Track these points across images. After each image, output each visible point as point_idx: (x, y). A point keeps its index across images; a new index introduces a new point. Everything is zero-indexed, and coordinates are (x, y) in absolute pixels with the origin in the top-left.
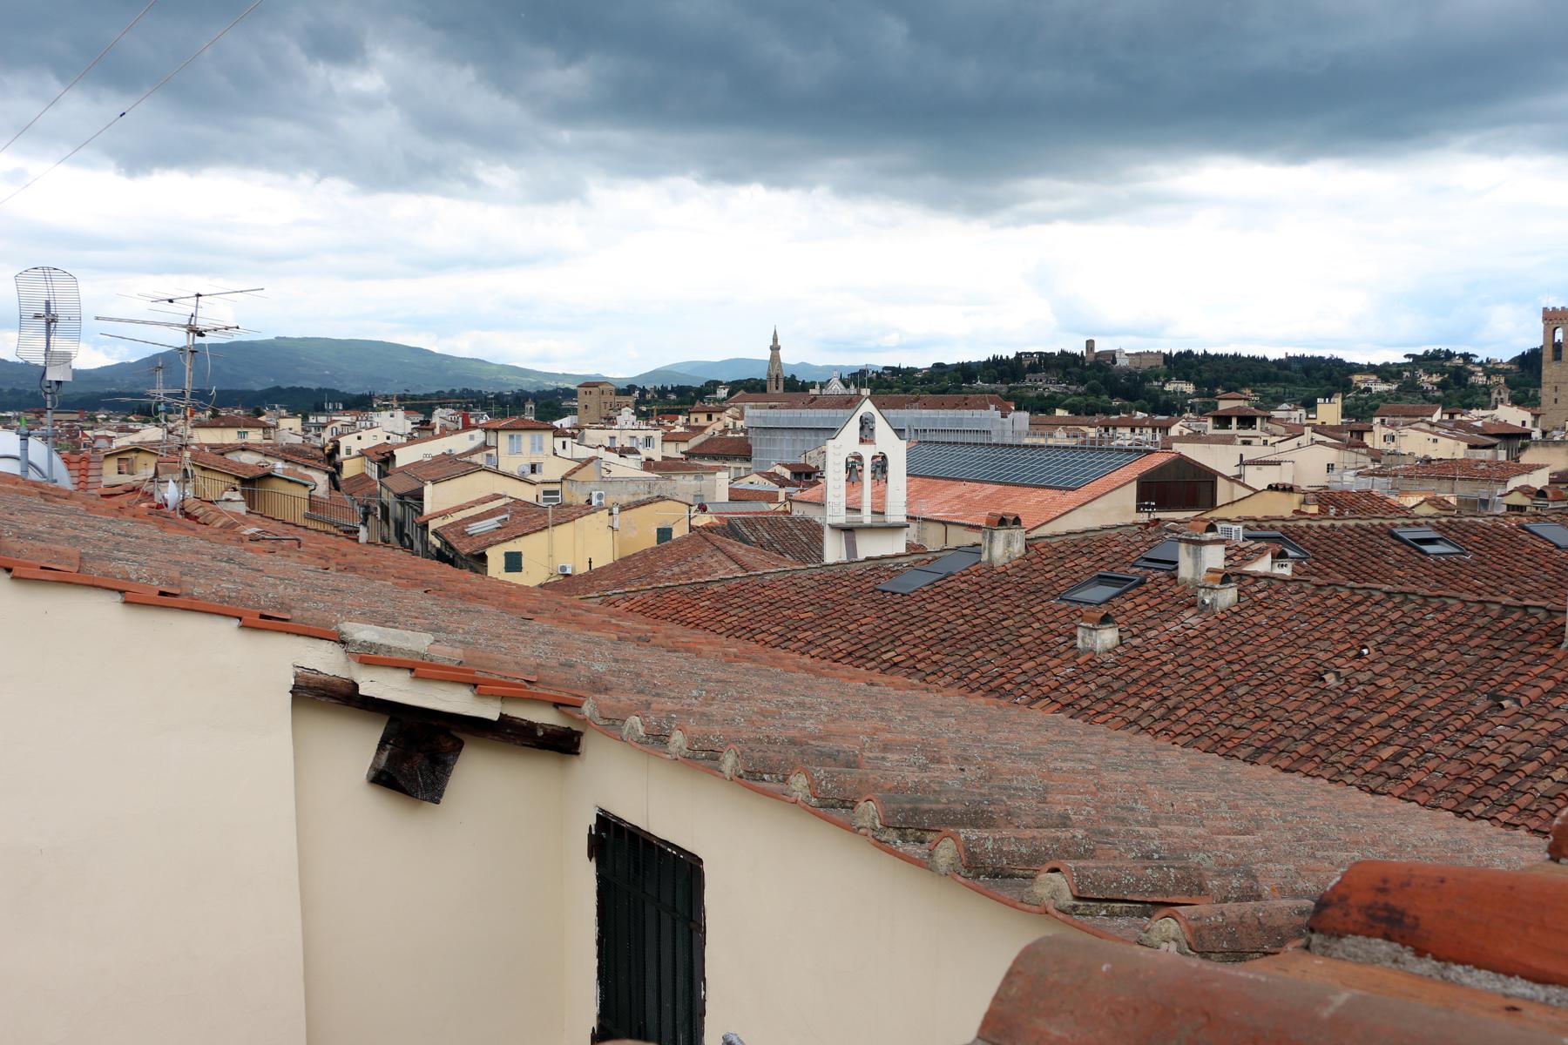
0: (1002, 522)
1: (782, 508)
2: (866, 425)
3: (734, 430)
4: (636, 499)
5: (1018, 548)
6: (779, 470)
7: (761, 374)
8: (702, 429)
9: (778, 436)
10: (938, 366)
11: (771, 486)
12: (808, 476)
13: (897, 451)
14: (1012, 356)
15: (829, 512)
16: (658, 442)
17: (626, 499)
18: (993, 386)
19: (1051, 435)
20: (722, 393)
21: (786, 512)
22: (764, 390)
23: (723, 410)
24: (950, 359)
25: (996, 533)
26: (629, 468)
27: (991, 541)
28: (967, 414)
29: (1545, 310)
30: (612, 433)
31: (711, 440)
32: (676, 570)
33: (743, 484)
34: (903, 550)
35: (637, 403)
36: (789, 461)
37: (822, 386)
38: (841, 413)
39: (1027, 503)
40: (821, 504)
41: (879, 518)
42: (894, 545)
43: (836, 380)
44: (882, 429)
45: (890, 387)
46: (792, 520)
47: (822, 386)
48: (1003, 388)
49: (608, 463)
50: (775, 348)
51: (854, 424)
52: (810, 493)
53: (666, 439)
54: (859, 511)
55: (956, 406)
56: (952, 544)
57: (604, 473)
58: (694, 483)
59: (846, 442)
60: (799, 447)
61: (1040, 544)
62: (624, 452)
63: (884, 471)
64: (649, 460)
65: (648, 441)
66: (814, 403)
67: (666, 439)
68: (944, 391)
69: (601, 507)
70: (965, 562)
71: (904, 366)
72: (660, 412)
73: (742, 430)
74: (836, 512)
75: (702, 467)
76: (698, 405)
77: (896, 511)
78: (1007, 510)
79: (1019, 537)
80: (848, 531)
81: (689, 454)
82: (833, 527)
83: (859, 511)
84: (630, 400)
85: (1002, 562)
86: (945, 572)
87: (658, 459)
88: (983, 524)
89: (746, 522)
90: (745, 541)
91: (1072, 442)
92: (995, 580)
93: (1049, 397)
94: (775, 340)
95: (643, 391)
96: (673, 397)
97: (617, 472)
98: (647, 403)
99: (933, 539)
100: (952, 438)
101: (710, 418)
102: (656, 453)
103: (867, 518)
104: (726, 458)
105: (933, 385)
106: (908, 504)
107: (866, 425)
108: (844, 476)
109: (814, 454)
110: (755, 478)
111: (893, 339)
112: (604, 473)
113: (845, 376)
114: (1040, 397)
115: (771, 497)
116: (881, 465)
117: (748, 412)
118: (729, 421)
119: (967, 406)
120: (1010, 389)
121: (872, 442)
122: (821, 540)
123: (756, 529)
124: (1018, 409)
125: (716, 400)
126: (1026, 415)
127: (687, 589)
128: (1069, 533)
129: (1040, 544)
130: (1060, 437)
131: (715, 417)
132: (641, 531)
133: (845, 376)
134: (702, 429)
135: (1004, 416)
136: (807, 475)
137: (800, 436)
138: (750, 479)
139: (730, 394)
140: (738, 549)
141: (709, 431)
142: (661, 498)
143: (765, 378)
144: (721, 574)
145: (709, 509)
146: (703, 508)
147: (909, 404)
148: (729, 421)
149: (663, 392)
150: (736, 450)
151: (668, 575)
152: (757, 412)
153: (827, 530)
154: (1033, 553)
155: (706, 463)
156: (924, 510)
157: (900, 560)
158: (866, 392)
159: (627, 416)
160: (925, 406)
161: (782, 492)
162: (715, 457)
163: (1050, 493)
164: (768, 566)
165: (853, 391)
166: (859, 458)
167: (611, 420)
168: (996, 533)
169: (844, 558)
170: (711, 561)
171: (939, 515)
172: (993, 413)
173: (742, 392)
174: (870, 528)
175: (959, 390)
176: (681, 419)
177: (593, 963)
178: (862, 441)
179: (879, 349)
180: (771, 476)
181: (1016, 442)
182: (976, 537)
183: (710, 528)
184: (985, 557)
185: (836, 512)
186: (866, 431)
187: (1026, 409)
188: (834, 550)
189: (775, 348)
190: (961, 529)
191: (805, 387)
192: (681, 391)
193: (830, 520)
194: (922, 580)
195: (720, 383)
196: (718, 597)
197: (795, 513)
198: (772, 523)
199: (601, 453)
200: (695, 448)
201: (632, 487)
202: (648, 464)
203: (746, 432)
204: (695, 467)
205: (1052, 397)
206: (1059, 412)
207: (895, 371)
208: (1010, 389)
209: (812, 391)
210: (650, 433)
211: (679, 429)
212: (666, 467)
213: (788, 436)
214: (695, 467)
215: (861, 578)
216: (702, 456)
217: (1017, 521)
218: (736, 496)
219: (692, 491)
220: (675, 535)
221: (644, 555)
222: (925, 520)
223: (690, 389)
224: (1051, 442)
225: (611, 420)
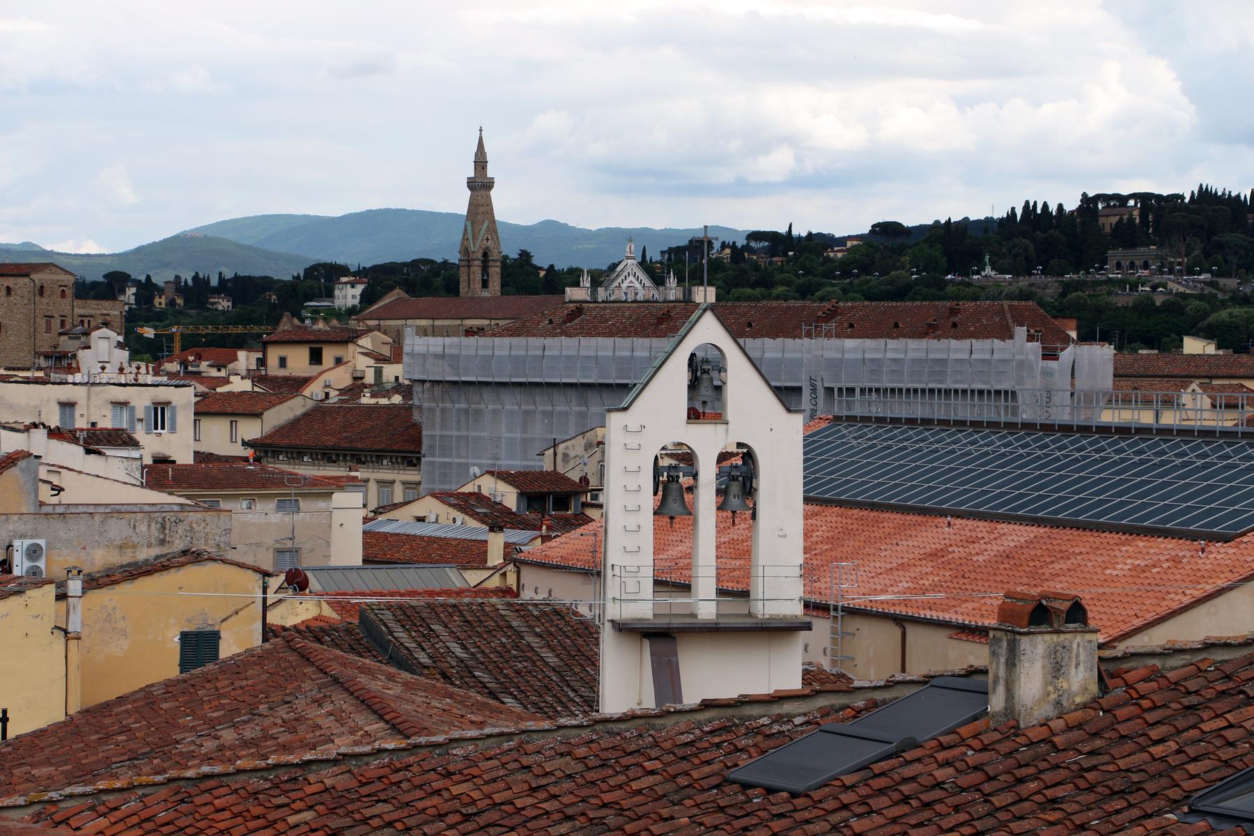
0: (1040, 615)
1: (495, 582)
2: (705, 383)
3: (379, 388)
4: (126, 559)
5: (1080, 680)
6: (488, 486)
7: (445, 249)
8: (297, 384)
9: (488, 403)
10: (887, 231)
11: (469, 527)
12: (562, 501)
13: (779, 441)
14: (1072, 205)
15: (612, 589)
16: (185, 418)
17: (100, 558)
18: (1024, 282)
19: (1168, 403)
20: (348, 295)
21: (505, 592)
22: (452, 288)
23: (350, 338)
24: (916, 212)
25: (1025, 643)
26: (109, 480)
27: (1012, 663)
28: (955, 349)
29: (1084, 195)
30: (65, 393)
31: (319, 413)
32: (228, 736)
33: (401, 522)
34: (794, 683)
35: (132, 320)
36: (515, 464)
37: (598, 279)
38: (642, 346)
39: (1112, 573)
40: (593, 572)
41: (734, 607)
42: (777, 672)
43: (631, 265)
44: (743, 386)
45: (766, 282)
46: (521, 610)
47: (598, 279)
48: (1048, 285)
49: (57, 469)
50: (480, 185)
51: (675, 375)
52: (566, 545)
53: (205, 409)
54: (686, 588)
55: (929, 331)
56: (916, 671)
57: (45, 493)
58: (276, 518)
59: (656, 417)
60: (538, 430)
61: (1136, 671)
62: (96, 441)
63: (749, 490)
64: (161, 461)
65: (160, 415)
66: (577, 321)
67: (205, 409)
68: (901, 293)
69: (36, 580)
70: (946, 714)
71: (800, 231)
72: (190, 343)
73: (398, 388)
74: (630, 594)
75: (295, 479)
76: (287, 324)
77: (780, 590)
78: (1058, 586)
79: (1081, 650)
80: (662, 638)
81: (264, 448)
82: (623, 628)
83: (686, 588)
84: (115, 310)
85: (1047, 710)
86: (897, 739)
87: (184, 457)
88: (991, 622)
89: (407, 616)
90: (402, 661)
91: (1228, 421)
92: (1024, 760)
93: (1167, 306)
94: (481, 162)
95: (147, 289)
96: (224, 304)
97: (77, 491)
98: (156, 318)
99: (872, 658)
100: (919, 409)
101: (316, 358)
102: (180, 445)
103: (706, 606)
104: (358, 457)
105: (874, 279)
106: (809, 572)
107: (705, 383)
108: (648, 501)
109: (576, 447)
110: (429, 507)
111: (779, 162)
112: (45, 493)
113: (654, 255)
114: (1144, 308)
115: (473, 555)
116: (740, 474)
117: (414, 343)
118: (364, 365)
119: (957, 330)
120: (1068, 288)
121: (718, 417)
122: (593, 661)
123: (431, 635)
124: (1086, 337)
125: (332, 313)
126: (1105, 352)
127: (256, 783)
128: (1209, 646)
129: (1136, 671)
130: (1195, 408)
131: (329, 354)
132: (140, 641)
133: (654, 255)
134: (297, 384)
135: (1050, 355)
136: (560, 501)
137: (541, 404)
138: (418, 509)
139: (368, 298)
140: (384, 683)
141: (315, 390)
142: (193, 557)
143: (454, 258)
144: (343, 745)
145: (314, 584)
146: (297, 581)
147: (813, 326)
148: (364, 365)
149: (197, 292)
150: (379, 438)
151: (207, 749)
152: (435, 344)
153: (608, 637)
154: (1119, 693)
155: (307, 470)
156: (849, 587)
157: (787, 708)
158: (705, 294)
159: (105, 349)
160: (852, 330)
161: (496, 544)
162: (328, 455)
163: (1168, 546)
164: (460, 725)
165: (673, 290)
166: (687, 458)
167: (61, 363)
168: (1025, 643)
169: (650, 703)
170: (317, 714)
171: (885, 599)
172: (1021, 346)
173: (397, 293)
174: (713, 631)
175: (936, 290)
176: (245, 359)
177: (409, 207)
178: (694, 415)
179: (743, 189)
180: (469, 503)
181: (1081, 419)
182: (975, 654)
183: (315, 631)
184: (997, 702)
185: (630, 594)
186: (705, 392)
187: (1105, 338)
188: (623, 684)
189: (480, 185)
190: (940, 636)
191: (556, 281)
192: (246, 290)
193: (614, 611)
194: (837, 759)
195: (342, 270)
196: (334, 801)
197: (527, 595)
198: (472, 617)
199: (38, 442)
200: (281, 431)
201: (117, 530)
202: (159, 472)
203: (407, 391)
204: (278, 480)
205: (1176, 306)
206: (1193, 346)
207: (779, 242)
208: (1068, 288)
209: (572, 293)
210: (164, 394)
211: (240, 385)
212: (207, 478)
213: (511, 403)
214: (278, 480)
215: (689, 752)
216: (298, 453)
217: (1077, 613)
218: (380, 550)
219: (270, 540)
220: (227, 649)
221: (147, 698)
222: (852, 612)
223: (264, 284)
224: (1169, 418)
225: (61, 363)
